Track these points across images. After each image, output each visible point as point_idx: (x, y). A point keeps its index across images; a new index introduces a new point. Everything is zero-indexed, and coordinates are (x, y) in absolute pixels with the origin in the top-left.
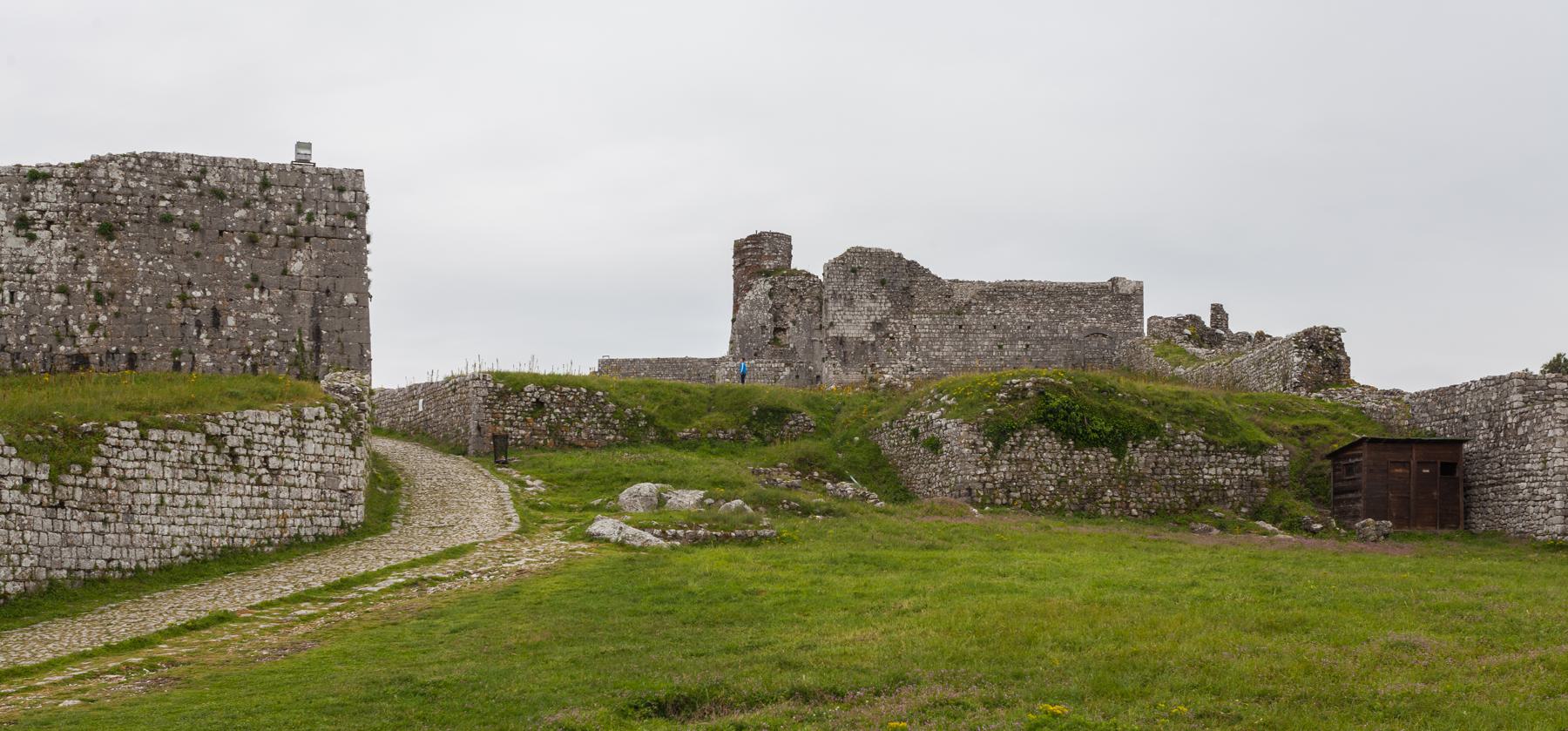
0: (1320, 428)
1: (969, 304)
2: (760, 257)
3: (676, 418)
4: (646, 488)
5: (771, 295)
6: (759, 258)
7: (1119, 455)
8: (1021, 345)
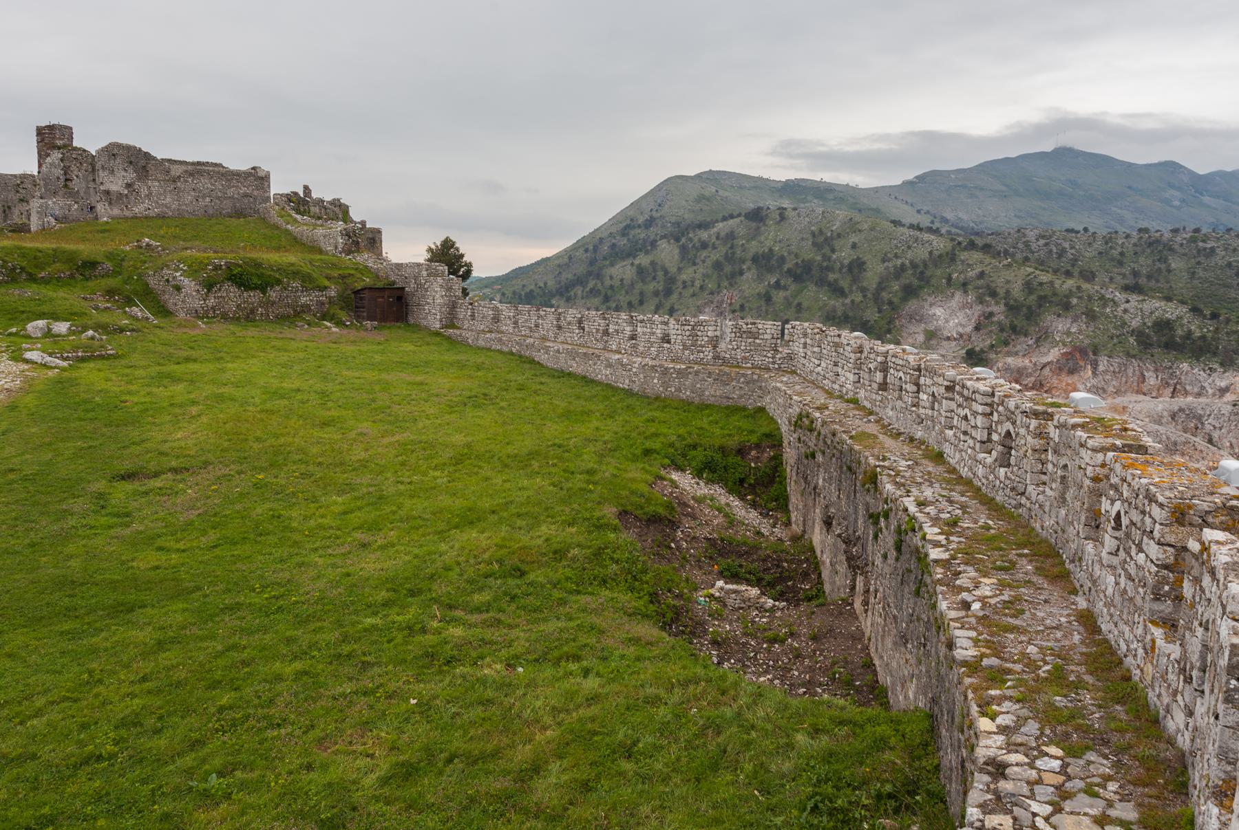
0: (350, 275)
1: (179, 177)
2: (54, 138)
3: (36, 266)
4: (41, 323)
5: (62, 160)
6: (52, 139)
7: (264, 293)
8: (208, 199)
